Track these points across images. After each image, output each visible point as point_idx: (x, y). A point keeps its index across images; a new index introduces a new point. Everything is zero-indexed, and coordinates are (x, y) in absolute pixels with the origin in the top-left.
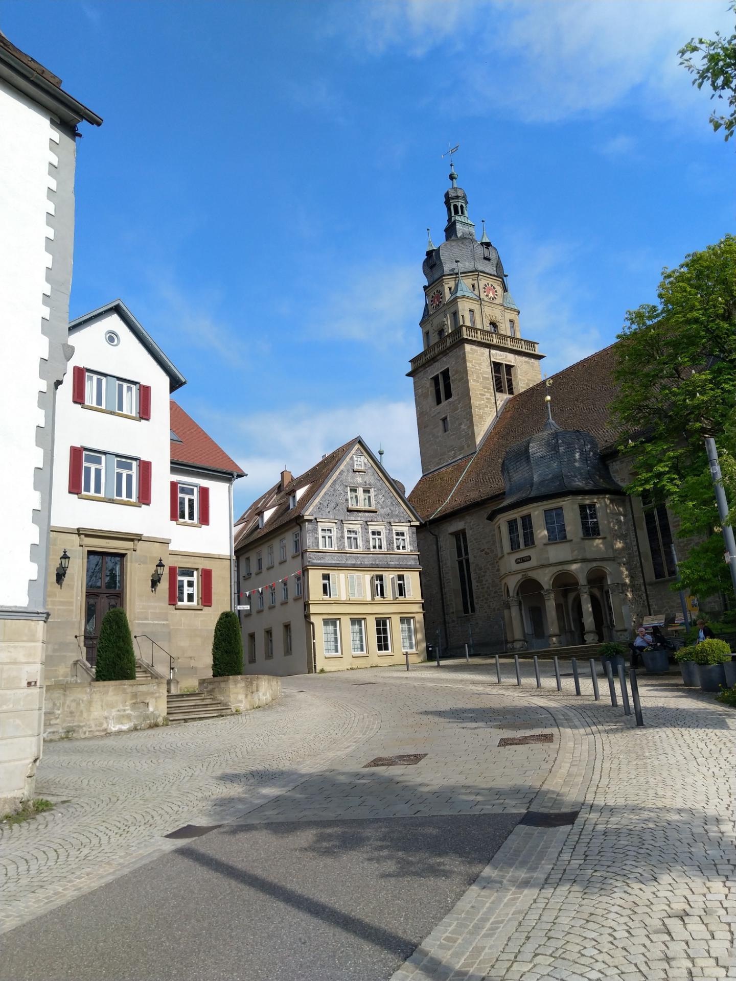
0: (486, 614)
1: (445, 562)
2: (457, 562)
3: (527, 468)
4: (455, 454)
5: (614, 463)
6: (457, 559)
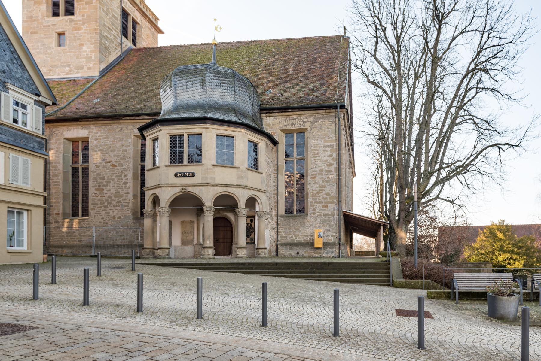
0: (102, 221)
1: (54, 164)
2: (71, 168)
3: (200, 91)
4: (70, 71)
5: (268, 118)
6: (71, 164)
